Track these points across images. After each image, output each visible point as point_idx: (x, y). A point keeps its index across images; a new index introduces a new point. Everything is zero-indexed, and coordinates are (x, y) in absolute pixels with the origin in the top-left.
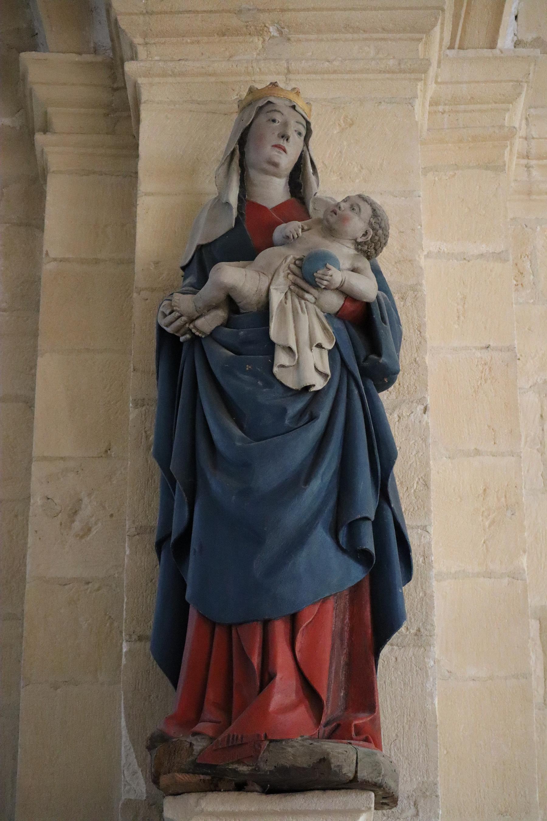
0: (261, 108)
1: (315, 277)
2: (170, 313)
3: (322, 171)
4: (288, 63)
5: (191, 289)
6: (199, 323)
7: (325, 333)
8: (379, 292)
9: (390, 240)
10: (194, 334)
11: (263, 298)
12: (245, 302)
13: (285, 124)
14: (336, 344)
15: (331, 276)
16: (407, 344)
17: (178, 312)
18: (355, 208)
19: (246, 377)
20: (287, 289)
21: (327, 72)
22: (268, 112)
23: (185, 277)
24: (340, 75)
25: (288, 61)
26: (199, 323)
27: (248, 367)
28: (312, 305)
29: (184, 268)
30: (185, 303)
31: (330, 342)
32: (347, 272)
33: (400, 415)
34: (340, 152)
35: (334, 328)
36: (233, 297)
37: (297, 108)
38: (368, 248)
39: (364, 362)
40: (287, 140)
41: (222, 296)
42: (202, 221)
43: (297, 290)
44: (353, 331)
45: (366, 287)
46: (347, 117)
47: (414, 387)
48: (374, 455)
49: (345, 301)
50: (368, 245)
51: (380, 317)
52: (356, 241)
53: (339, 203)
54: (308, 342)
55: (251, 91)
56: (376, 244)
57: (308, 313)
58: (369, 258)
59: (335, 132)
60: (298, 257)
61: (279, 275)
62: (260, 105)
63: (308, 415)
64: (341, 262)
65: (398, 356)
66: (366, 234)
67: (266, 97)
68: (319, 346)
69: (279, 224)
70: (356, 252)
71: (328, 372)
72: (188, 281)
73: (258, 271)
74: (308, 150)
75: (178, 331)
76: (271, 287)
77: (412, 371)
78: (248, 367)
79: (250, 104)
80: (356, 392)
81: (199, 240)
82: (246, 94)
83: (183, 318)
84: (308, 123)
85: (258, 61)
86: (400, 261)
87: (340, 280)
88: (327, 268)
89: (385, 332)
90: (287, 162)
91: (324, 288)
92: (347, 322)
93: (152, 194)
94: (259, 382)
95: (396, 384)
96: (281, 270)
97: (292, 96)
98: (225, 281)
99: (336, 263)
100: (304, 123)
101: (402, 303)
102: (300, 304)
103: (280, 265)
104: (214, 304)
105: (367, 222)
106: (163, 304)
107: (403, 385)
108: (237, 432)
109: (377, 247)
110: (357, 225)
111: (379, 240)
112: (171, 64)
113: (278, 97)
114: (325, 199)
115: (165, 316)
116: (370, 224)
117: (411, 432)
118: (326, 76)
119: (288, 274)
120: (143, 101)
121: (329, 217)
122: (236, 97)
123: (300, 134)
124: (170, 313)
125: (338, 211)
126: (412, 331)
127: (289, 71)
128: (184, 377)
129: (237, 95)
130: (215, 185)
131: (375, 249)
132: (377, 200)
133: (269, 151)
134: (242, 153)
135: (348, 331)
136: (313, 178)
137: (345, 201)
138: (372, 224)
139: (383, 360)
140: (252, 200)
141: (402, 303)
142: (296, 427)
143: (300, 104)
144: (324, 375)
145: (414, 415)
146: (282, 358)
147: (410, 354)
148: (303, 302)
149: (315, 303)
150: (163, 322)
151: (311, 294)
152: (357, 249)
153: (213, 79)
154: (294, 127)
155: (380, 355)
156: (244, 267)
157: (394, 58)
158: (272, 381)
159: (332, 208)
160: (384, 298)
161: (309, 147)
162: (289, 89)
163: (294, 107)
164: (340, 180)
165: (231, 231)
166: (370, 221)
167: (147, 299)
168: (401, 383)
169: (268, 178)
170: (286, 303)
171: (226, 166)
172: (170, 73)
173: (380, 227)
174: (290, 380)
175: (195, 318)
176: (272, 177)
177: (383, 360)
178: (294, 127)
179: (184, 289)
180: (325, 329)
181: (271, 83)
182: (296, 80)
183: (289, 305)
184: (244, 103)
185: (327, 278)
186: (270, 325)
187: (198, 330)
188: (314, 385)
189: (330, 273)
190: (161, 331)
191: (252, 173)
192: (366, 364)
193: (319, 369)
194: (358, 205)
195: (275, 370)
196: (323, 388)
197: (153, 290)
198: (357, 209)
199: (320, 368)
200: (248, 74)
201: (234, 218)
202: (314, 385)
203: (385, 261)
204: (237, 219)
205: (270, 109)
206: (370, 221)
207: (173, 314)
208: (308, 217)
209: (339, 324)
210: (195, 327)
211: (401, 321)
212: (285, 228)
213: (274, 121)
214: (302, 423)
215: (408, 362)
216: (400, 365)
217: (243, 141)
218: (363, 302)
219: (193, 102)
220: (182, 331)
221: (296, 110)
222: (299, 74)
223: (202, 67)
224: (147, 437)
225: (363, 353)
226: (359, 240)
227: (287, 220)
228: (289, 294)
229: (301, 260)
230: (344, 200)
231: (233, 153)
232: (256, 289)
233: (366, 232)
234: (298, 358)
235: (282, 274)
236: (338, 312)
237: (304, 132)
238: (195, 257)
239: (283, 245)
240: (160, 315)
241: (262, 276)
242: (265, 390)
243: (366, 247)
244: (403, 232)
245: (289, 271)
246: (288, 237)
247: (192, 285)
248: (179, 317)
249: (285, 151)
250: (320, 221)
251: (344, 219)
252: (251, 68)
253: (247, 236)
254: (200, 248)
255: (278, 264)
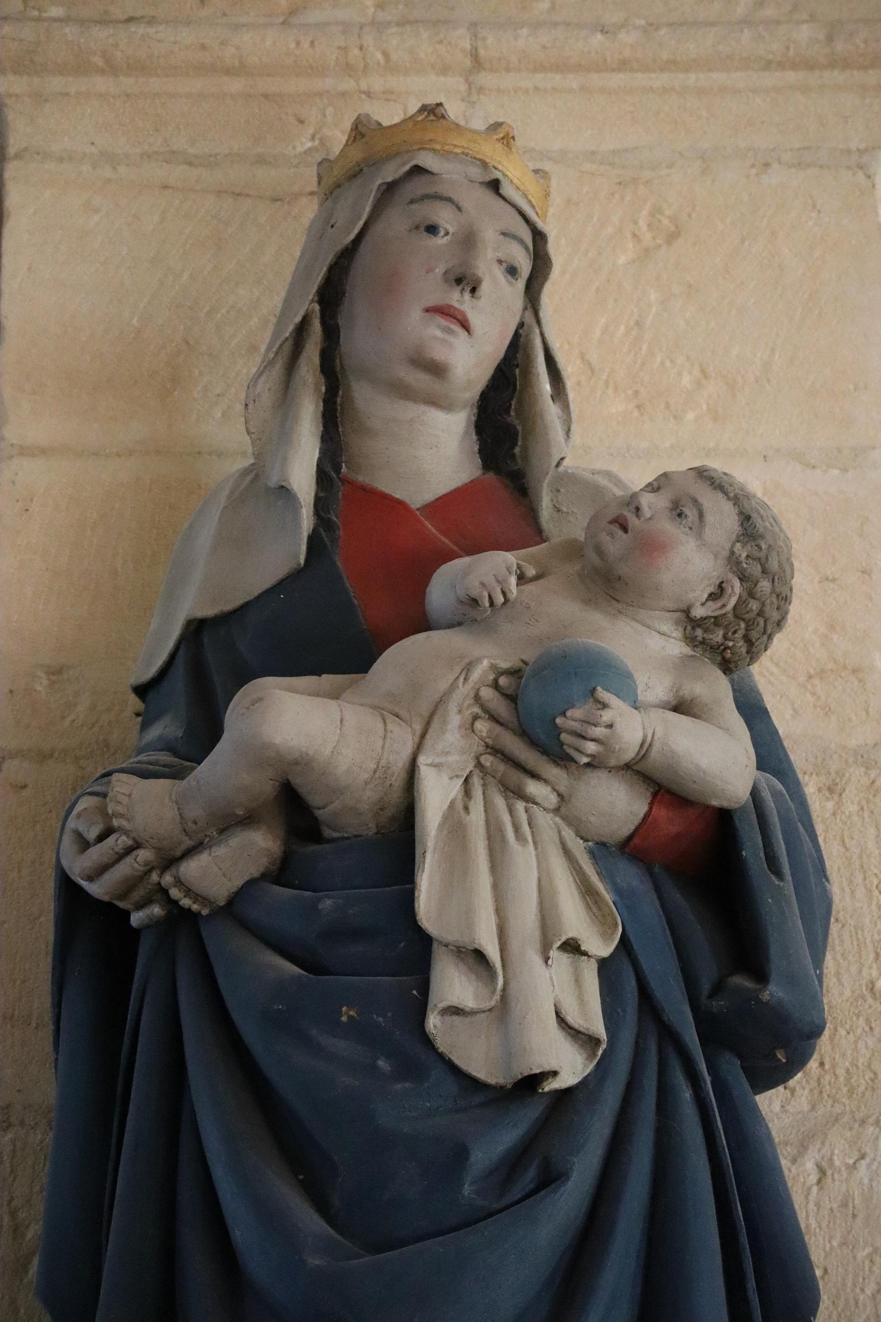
0: (390, 189)
1: (557, 731)
2: (101, 838)
3: (579, 383)
4: (475, 36)
5: (165, 757)
6: (191, 868)
7: (587, 904)
8: (760, 774)
9: (795, 609)
10: (175, 903)
11: (396, 796)
12: (337, 805)
13: (468, 241)
14: (624, 941)
15: (610, 726)
16: (846, 936)
17: (127, 833)
18: (687, 511)
19: (341, 1046)
20: (471, 766)
21: (601, 67)
22: (412, 202)
23: (147, 720)
24: (639, 75)
25: (473, 26)
26: (193, 869)
27: (347, 1013)
28: (550, 816)
29: (141, 691)
30: (149, 805)
31: (606, 937)
32: (661, 715)
33: (824, 1164)
34: (637, 323)
35: (617, 890)
36: (302, 791)
37: (507, 189)
38: (725, 637)
39: (711, 996)
40: (473, 290)
41: (264, 785)
42: (205, 540)
43: (502, 767)
44: (677, 897)
45: (719, 761)
46: (660, 211)
47: (869, 1075)
48: (746, 1301)
49: (651, 804)
50: (726, 627)
51: (762, 855)
52: (688, 617)
53: (634, 496)
54: (537, 935)
55: (361, 130)
56: (750, 625)
57: (535, 843)
58: (727, 667)
59: (622, 260)
60: (504, 665)
61: (445, 722)
62: (390, 179)
63: (533, 1168)
64: (641, 678)
65: (820, 978)
66: (719, 593)
67: (408, 152)
68: (572, 947)
69: (449, 556)
70: (687, 650)
71: (599, 1028)
72: (155, 732)
73: (375, 707)
74: (538, 322)
75: (124, 895)
76: (422, 760)
77: (861, 1021)
78: (347, 1013)
79: (355, 174)
80: (687, 1095)
81: (193, 603)
82: (344, 139)
83: (144, 855)
84: (539, 236)
85: (380, 27)
86: (823, 671)
87: (638, 737)
88: (597, 701)
89: (778, 902)
90: (471, 360)
91: (588, 765)
92: (657, 869)
93: (43, 452)
94: (381, 1063)
95: (813, 1064)
96: (452, 707)
97: (491, 151)
98: (278, 740)
99: (623, 684)
100: (527, 236)
101: (830, 805)
102: (511, 811)
103: (453, 687)
104: (240, 812)
105: (726, 553)
106: (79, 807)
107: (834, 1067)
108: (310, 1221)
109: (754, 635)
110: (692, 565)
111: (760, 613)
112: (101, 34)
113: (446, 155)
114: (588, 476)
115: (84, 845)
116: (732, 560)
117: (859, 1221)
118: (596, 80)
119: (476, 718)
120: (11, 151)
121: (605, 538)
122: (309, 144)
123: (512, 271)
124: (101, 838)
125: (633, 521)
126: (860, 893)
127: (477, 62)
128: (141, 1039)
129: (313, 138)
130: (236, 421)
131: (747, 639)
132: (752, 479)
133: (416, 327)
134: (329, 330)
135: (660, 897)
136: (552, 411)
137: (653, 488)
138: (738, 563)
139: (774, 991)
140: (361, 479)
141: (830, 805)
142: (496, 1206)
143: (514, 172)
144: (583, 1039)
145: (869, 1166)
146: (453, 986)
147: (854, 969)
148: (520, 806)
149: (557, 811)
150: (77, 866)
151: (546, 782)
152: (690, 640)
153: (236, 85)
154: (497, 253)
155: (761, 977)
156: (335, 695)
157: (813, 18)
158: (421, 1057)
159: (612, 513)
160: (775, 794)
161: (541, 315)
162: (479, 124)
163: (495, 185)
164: (636, 413)
165: (292, 581)
166: (732, 553)
167: (25, 787)
168: (827, 1060)
169: (413, 410)
170: (466, 809)
171: (279, 367)
172: (98, 61)
173: (764, 571)
174: (478, 1056)
175: (178, 853)
176: (423, 408)
177: (774, 991)
178: (497, 253)
179: (143, 757)
180: (587, 891)
181: (424, 108)
182: (499, 90)
183: (477, 817)
184: (338, 172)
185: (599, 732)
186: (418, 880)
187: (188, 892)
188: (555, 1074)
189: (606, 716)
190: (69, 892)
191: (364, 397)
192: (719, 1005)
193: (570, 1019)
194: (695, 501)
195: (433, 1022)
196: (584, 1083)
197: (44, 757)
198: (691, 513)
199: (574, 1018)
200: (348, 69)
201: (305, 535)
202: (555, 1074)
203: (775, 670)
204: (314, 540)
205: (420, 192)
206: (732, 553)
207: (110, 840)
208: (538, 535)
209: (631, 875)
210: (179, 882)
211: (828, 864)
212: (466, 572)
213: (432, 229)
214: (517, 1192)
215: (848, 993)
216: (825, 1001)
217: (332, 293)
218: (708, 807)
219: (171, 156)
220: (137, 895)
221: (504, 198)
222: (508, 70)
223: (203, 47)
224: (17, 1231)
225: (707, 973)
226: (699, 612)
227: (474, 549)
228: (476, 781)
229: (515, 673)
230: (650, 484)
231: (302, 329)
232: (373, 766)
233: (721, 587)
234: (506, 984)
235: (455, 720)
236: (631, 837)
237: (525, 266)
238: (181, 653)
239: (460, 624)
240: (68, 841)
241: (394, 726)
242: (399, 1086)
243: (721, 633)
244: (834, 580)
245: (476, 710)
246: (474, 602)
247: (169, 747)
248: (129, 851)
249: (466, 326)
250: (573, 551)
251: (651, 547)
252: (356, 51)
253: (343, 601)
254: (196, 630)
255: (443, 685)
